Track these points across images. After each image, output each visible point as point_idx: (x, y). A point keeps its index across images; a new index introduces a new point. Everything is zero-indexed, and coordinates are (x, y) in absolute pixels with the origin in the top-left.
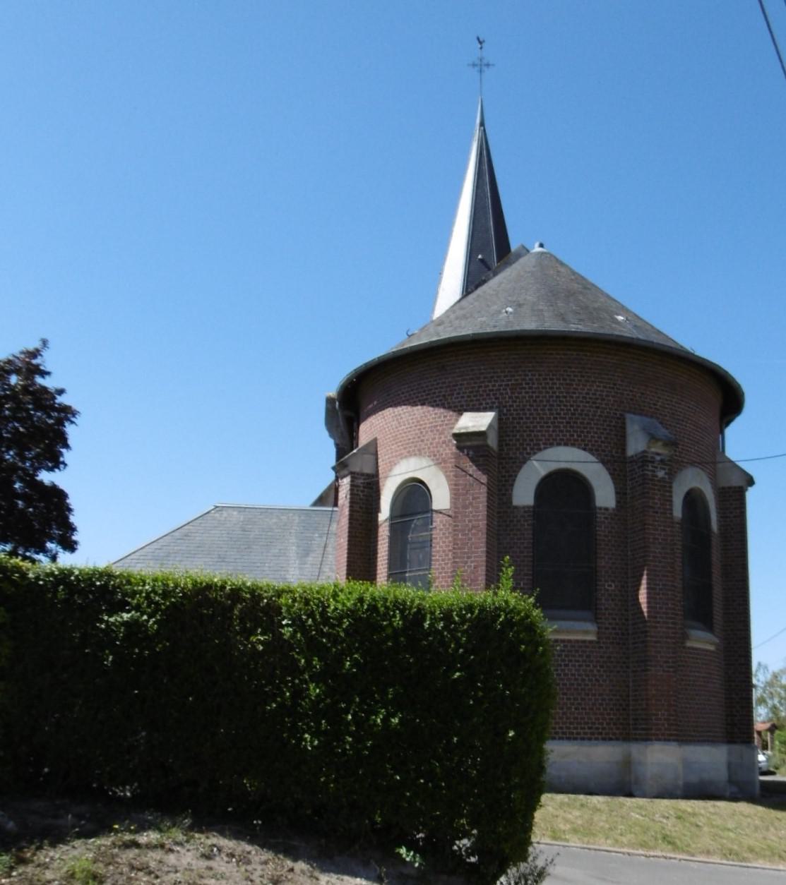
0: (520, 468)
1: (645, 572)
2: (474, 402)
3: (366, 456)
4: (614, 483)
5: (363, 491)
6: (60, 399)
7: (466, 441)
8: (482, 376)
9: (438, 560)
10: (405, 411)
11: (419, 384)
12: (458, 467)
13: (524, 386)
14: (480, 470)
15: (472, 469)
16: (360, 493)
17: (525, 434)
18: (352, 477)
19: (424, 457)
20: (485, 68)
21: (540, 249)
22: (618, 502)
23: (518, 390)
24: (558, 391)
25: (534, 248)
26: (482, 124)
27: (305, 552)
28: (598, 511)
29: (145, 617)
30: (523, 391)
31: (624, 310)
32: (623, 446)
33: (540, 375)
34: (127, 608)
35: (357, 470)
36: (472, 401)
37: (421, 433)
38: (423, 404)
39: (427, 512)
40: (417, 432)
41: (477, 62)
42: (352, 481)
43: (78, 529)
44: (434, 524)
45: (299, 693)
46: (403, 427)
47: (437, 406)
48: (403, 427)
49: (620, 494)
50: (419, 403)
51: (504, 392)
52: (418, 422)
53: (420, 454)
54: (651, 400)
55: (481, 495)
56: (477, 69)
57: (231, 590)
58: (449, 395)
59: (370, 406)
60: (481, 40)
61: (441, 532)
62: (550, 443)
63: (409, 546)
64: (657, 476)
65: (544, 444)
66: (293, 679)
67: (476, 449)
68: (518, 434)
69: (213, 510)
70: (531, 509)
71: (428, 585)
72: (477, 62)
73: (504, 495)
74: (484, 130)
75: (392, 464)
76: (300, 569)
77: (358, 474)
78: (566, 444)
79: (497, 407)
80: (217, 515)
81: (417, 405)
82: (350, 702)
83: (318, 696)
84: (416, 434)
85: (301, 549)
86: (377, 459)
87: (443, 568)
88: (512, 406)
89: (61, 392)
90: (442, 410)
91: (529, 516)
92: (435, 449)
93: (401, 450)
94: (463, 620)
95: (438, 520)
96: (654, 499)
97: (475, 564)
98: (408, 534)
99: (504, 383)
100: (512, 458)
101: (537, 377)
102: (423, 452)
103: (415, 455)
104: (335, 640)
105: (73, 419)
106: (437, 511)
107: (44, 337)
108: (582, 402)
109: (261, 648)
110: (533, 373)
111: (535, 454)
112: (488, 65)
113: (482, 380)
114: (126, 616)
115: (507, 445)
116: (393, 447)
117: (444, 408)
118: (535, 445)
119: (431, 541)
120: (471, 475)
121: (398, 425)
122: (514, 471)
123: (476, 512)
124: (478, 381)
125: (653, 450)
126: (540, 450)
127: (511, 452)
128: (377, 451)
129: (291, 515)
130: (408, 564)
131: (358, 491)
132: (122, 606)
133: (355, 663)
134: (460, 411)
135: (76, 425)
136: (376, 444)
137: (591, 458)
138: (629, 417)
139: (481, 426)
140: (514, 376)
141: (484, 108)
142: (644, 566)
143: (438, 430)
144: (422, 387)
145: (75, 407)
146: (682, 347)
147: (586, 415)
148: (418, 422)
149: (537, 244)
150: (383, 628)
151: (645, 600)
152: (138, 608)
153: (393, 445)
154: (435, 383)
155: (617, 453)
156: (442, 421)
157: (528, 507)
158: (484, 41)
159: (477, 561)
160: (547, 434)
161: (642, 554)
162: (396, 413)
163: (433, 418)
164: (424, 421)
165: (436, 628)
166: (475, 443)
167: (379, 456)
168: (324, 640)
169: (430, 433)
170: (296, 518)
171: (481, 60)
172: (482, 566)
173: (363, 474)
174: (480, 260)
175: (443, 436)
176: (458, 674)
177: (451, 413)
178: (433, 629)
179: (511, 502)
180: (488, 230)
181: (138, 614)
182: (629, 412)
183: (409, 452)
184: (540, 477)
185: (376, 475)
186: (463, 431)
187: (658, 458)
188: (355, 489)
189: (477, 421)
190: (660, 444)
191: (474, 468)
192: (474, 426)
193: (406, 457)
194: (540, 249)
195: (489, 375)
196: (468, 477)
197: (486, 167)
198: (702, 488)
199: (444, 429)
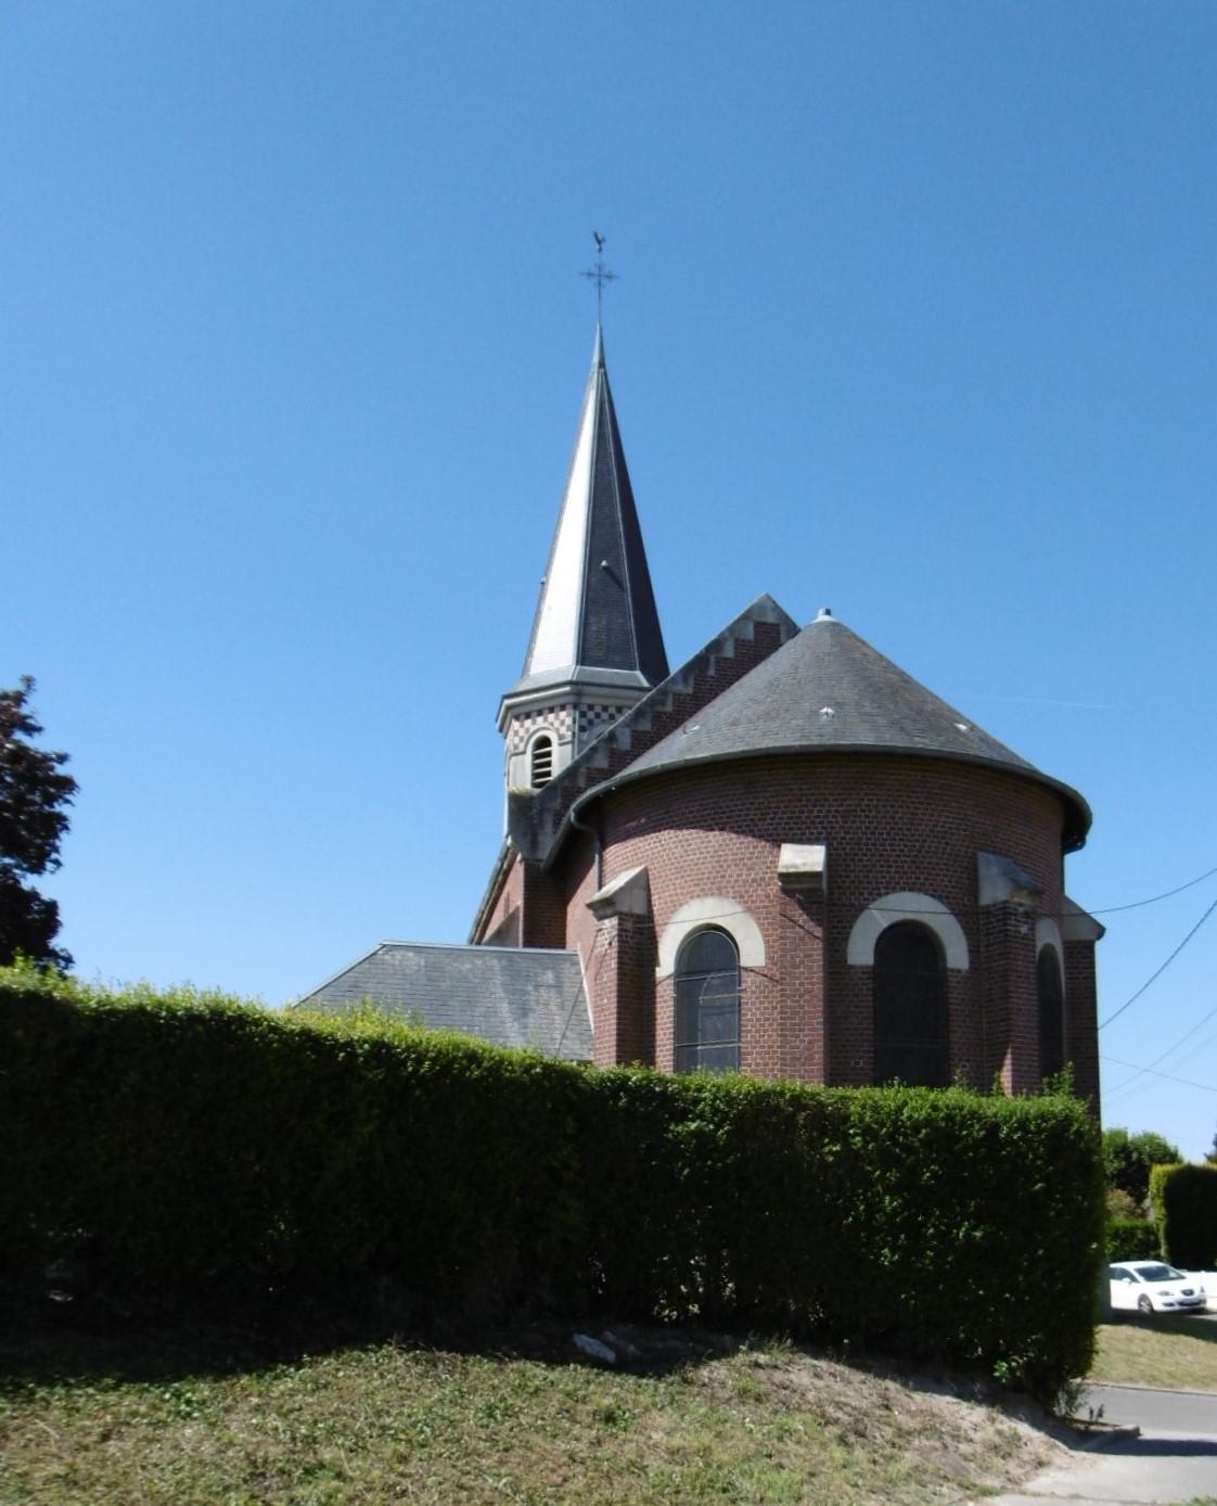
0: (855, 917)
1: (1009, 1050)
2: (795, 831)
3: (635, 891)
4: (968, 939)
5: (632, 938)
6: (61, 770)
7: (793, 883)
8: (804, 798)
9: (750, 1031)
10: (694, 835)
11: (716, 803)
12: (785, 916)
13: (859, 813)
14: (812, 920)
15: (802, 918)
16: (629, 939)
17: (861, 874)
18: (620, 919)
19: (727, 897)
20: (605, 282)
21: (827, 618)
22: (971, 962)
23: (852, 819)
24: (900, 821)
25: (816, 617)
26: (602, 364)
27: (523, 1012)
28: (949, 973)
29: (711, 1127)
30: (858, 820)
31: (966, 722)
32: (974, 892)
33: (879, 800)
34: (690, 1116)
35: (625, 909)
36: (791, 829)
37: (721, 866)
38: (722, 829)
39: (733, 969)
40: (714, 864)
41: (594, 270)
42: (620, 924)
43: (74, 959)
44: (744, 986)
45: (873, 1208)
46: (691, 857)
47: (743, 832)
48: (691, 857)
49: (973, 951)
50: (716, 828)
51: (834, 820)
52: (715, 852)
53: (720, 894)
54: (1004, 834)
55: (816, 950)
56: (594, 280)
57: (792, 1096)
58: (760, 820)
59: (633, 824)
60: (600, 237)
61: (754, 996)
62: (892, 888)
63: (700, 1011)
64: (1020, 933)
65: (884, 888)
66: (866, 1191)
67: (807, 893)
68: (853, 875)
69: (380, 949)
70: (871, 970)
71: (734, 1059)
72: (594, 270)
73: (837, 951)
74: (605, 373)
75: (676, 906)
76: (524, 1034)
77: (626, 915)
78: (911, 890)
79: (825, 839)
80: (386, 957)
81: (713, 830)
82: (928, 1215)
83: (894, 1209)
84: (714, 867)
85: (514, 1006)
86: (649, 896)
87: (757, 1042)
88: (844, 838)
89: (62, 759)
90: (750, 839)
91: (867, 979)
92: (743, 889)
93: (690, 886)
94: (1039, 1131)
95: (748, 980)
96: (1018, 960)
97: (811, 1038)
98: (699, 995)
99: (832, 809)
100: (845, 905)
101: (875, 803)
102: (724, 891)
103: (712, 894)
104: (908, 1149)
105: (68, 797)
106: (746, 969)
107: (28, 673)
108: (929, 836)
109: (831, 1159)
110: (871, 797)
111: (874, 900)
112: (610, 277)
113: (804, 803)
114: (693, 1126)
115: (839, 888)
116: (678, 882)
117: (754, 836)
118: (873, 889)
119: (740, 1005)
120: (800, 926)
121: (684, 854)
122: (849, 922)
123: (810, 973)
124: (799, 804)
125: (1016, 900)
126: (880, 895)
127: (844, 897)
128: (649, 886)
129: (487, 958)
130: (700, 1034)
131: (626, 936)
132: (682, 1116)
133: (934, 1175)
134: (777, 841)
135: (73, 805)
136: (648, 875)
137: (941, 908)
138: (982, 857)
139: (814, 864)
140: (845, 800)
141: (605, 344)
142: (1007, 1043)
143: (745, 865)
144: (721, 808)
145: (77, 780)
146: (1029, 764)
147: (934, 852)
148: (715, 852)
149: (821, 611)
150: (961, 1138)
151: (1010, 1085)
152: (701, 1116)
153: (676, 879)
154: (739, 803)
155: (969, 900)
156: (751, 853)
157: (867, 967)
158: (604, 240)
159: (813, 1035)
160: (888, 875)
161: (1004, 1028)
162: (680, 838)
163: (737, 849)
164: (724, 851)
165: (1012, 1138)
166: (805, 886)
167: (652, 892)
168: (897, 1150)
169: (733, 867)
170: (495, 962)
171: (600, 269)
172: (818, 1041)
173: (632, 915)
174: (604, 568)
175: (753, 873)
176: (1040, 1185)
177: (763, 843)
178: (1009, 1141)
179: (846, 961)
180: (615, 524)
181: (705, 1123)
182: (982, 850)
183: (703, 890)
184: (881, 929)
185: (649, 917)
186: (791, 870)
187: (1021, 909)
188: (624, 934)
189: (806, 857)
190: (1025, 892)
191: (805, 917)
192: (804, 864)
193: (699, 896)
194: (827, 618)
195: (813, 798)
196: (798, 929)
197: (609, 429)
198: (1055, 944)
199: (755, 864)
